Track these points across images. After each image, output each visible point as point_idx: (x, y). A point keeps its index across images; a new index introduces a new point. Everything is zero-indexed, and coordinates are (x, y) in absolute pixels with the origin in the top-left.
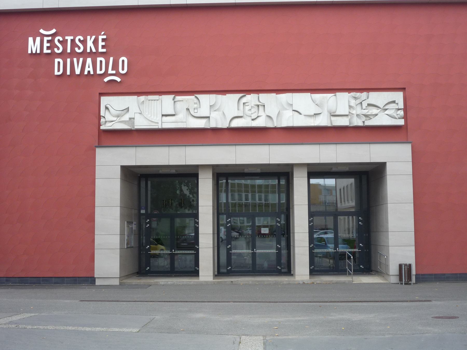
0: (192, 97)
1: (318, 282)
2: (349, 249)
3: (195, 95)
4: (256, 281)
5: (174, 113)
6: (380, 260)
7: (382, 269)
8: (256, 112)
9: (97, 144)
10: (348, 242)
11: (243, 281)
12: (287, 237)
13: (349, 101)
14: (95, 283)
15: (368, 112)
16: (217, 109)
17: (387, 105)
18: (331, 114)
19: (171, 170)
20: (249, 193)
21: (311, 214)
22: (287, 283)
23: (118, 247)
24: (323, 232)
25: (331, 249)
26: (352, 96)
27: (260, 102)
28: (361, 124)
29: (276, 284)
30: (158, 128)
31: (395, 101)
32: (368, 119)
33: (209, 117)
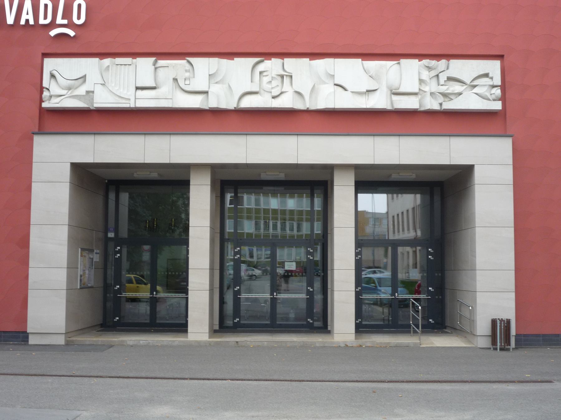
0: (183, 62)
1: (369, 345)
2: (407, 294)
3: (187, 58)
4: (273, 341)
5: (154, 85)
6: (461, 312)
7: (463, 326)
8: (279, 85)
9: (37, 127)
10: (410, 286)
11: (254, 341)
12: (323, 276)
13: (419, 72)
14: (28, 341)
15: (448, 89)
16: (220, 80)
17: (477, 80)
18: (391, 91)
19: (150, 172)
20: (278, 220)
21: (360, 244)
22: (321, 345)
23: (64, 286)
24: (371, 271)
25: (385, 293)
26: (424, 64)
27: (286, 71)
28: (436, 107)
29: (304, 346)
30: (130, 107)
31: (489, 73)
32: (446, 100)
33: (206, 93)
